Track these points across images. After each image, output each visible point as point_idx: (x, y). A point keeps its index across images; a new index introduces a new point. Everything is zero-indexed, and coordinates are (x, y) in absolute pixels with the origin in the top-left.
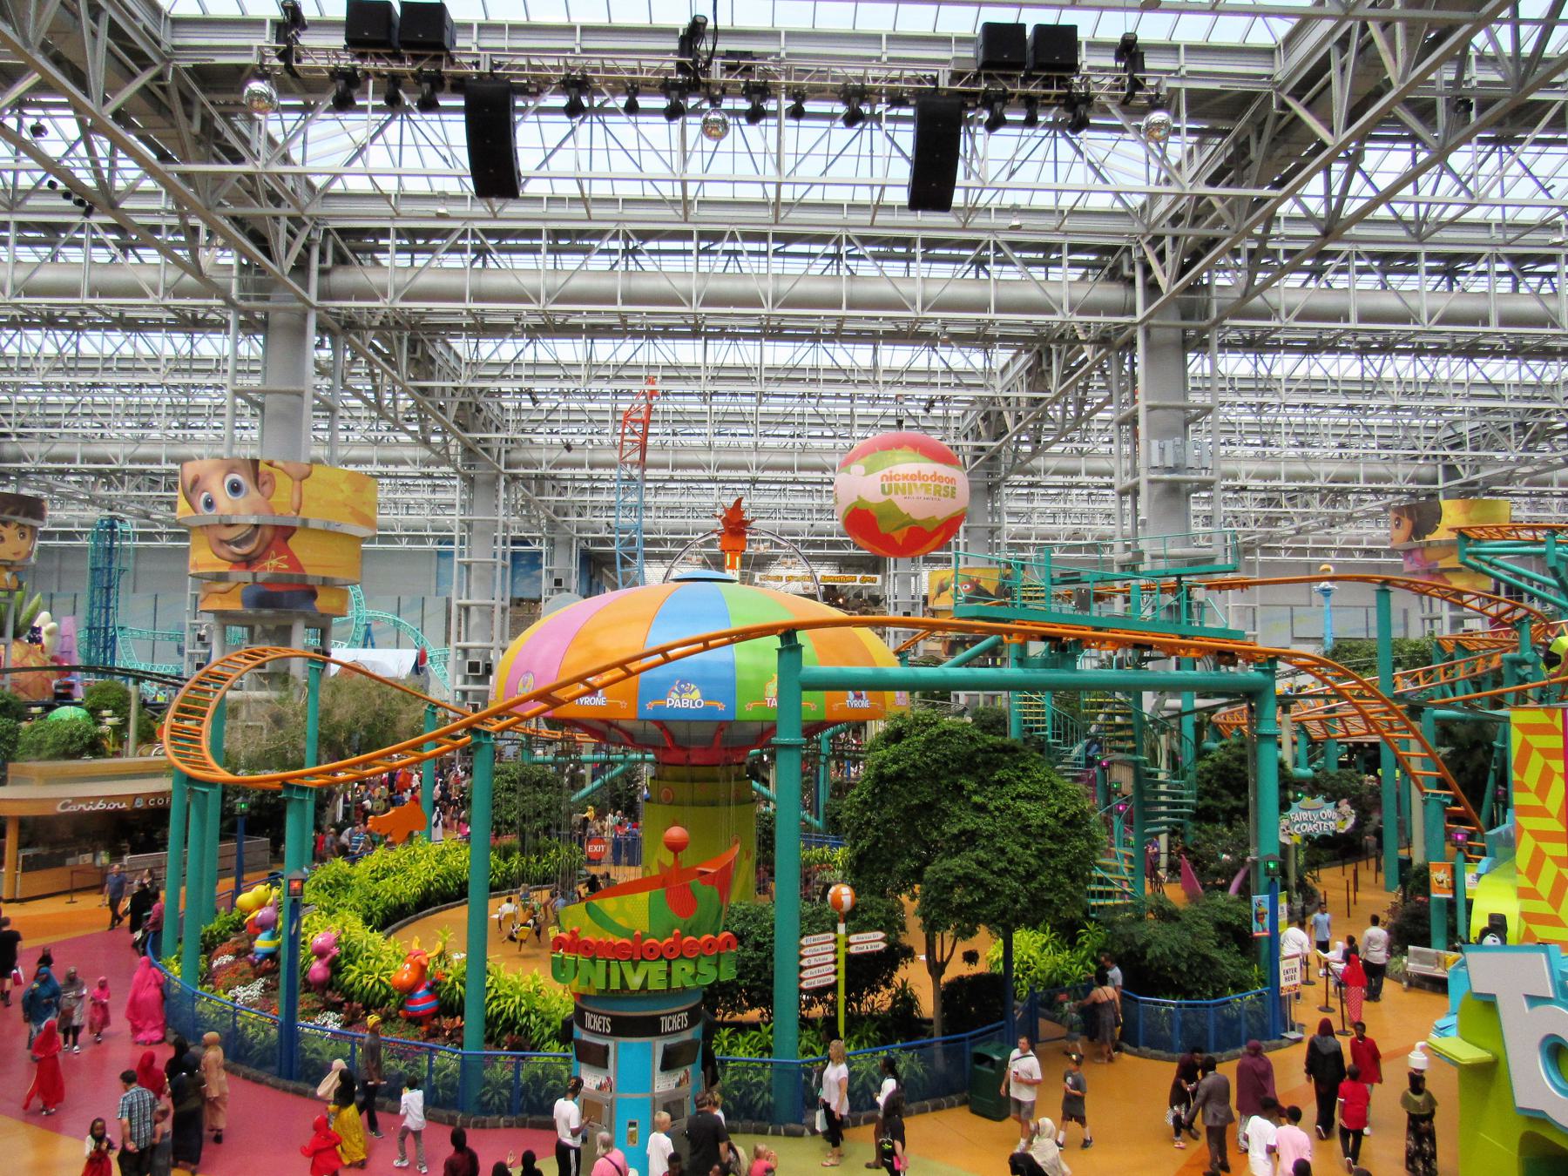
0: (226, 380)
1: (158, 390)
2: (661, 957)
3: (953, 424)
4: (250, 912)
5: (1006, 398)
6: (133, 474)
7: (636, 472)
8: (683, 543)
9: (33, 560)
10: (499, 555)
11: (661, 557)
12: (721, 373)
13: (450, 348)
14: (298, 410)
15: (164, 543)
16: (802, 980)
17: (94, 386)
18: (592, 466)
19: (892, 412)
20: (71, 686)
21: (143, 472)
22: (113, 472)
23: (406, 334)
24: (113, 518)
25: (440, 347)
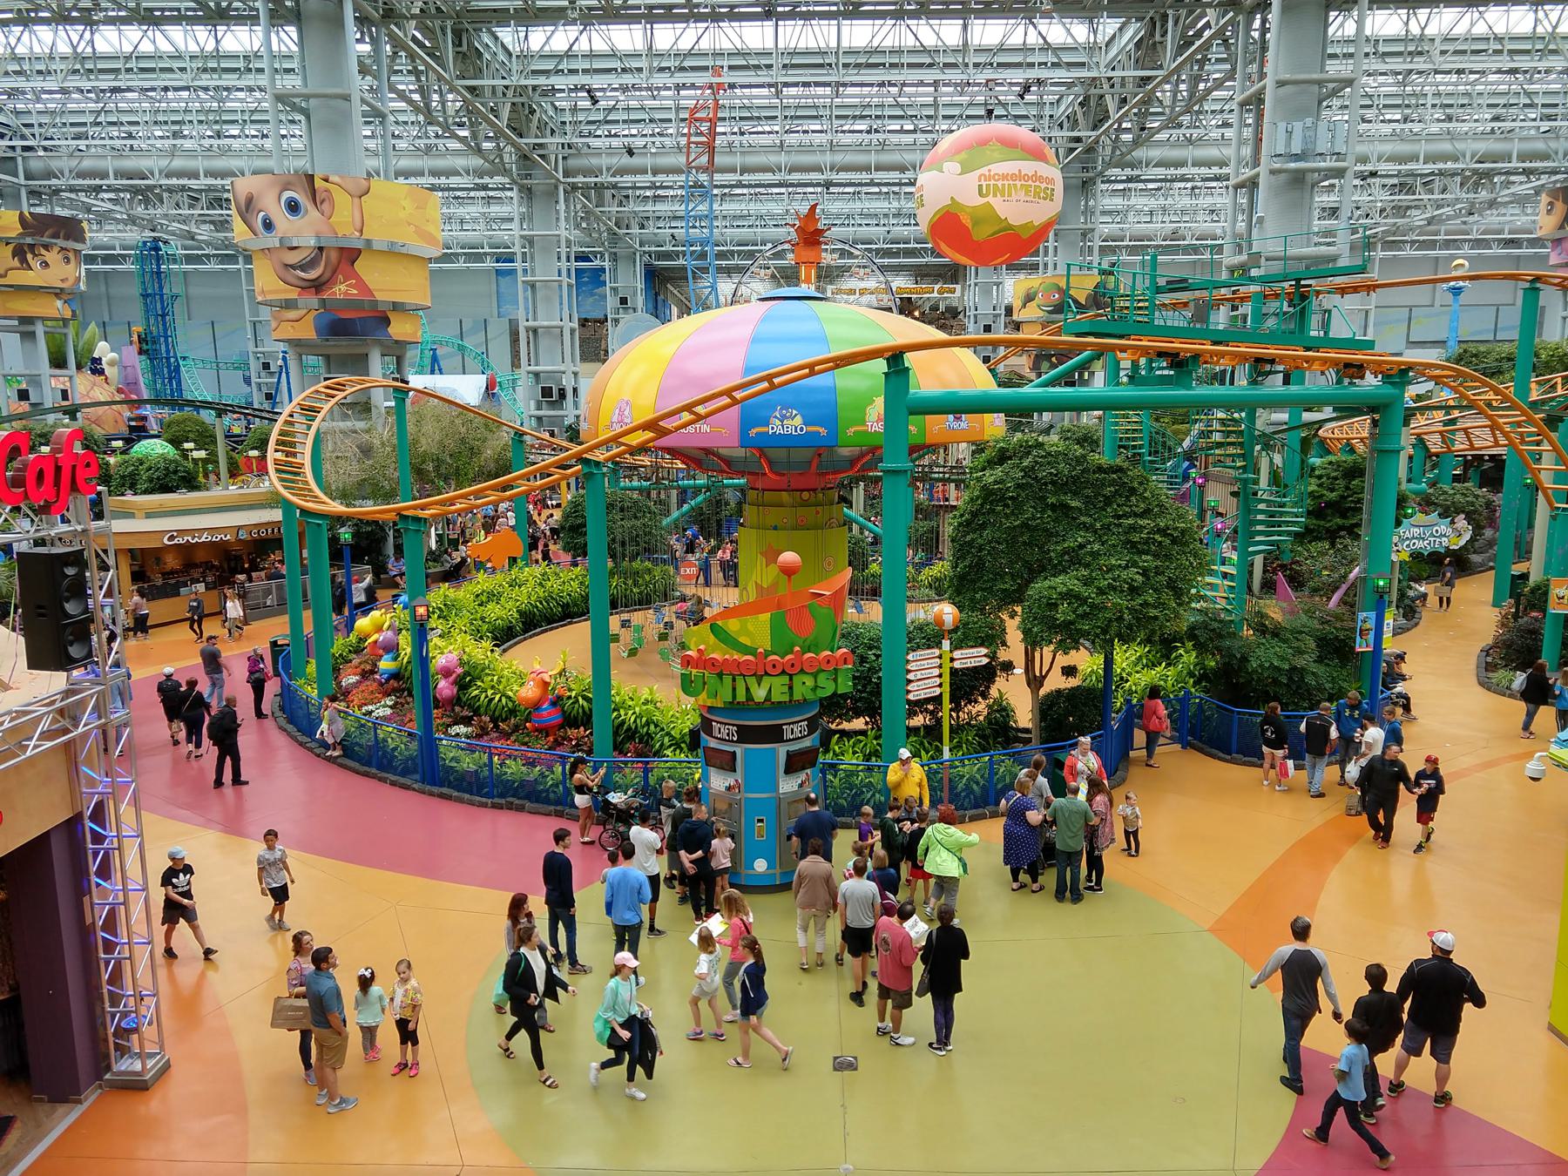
0: (263, 80)
1: (185, 94)
2: (783, 672)
3: (1047, 111)
4: (369, 636)
5: (1110, 79)
6: (170, 190)
7: (703, 177)
8: (750, 255)
9: (83, 287)
10: (564, 273)
11: (728, 271)
12: (796, 61)
13: (496, 38)
14: (347, 116)
15: (213, 266)
16: (909, 692)
17: (115, 90)
18: (655, 173)
19: (981, 99)
20: (145, 418)
21: (183, 189)
22: (150, 188)
23: (449, 23)
24: (156, 240)
25: (486, 39)
